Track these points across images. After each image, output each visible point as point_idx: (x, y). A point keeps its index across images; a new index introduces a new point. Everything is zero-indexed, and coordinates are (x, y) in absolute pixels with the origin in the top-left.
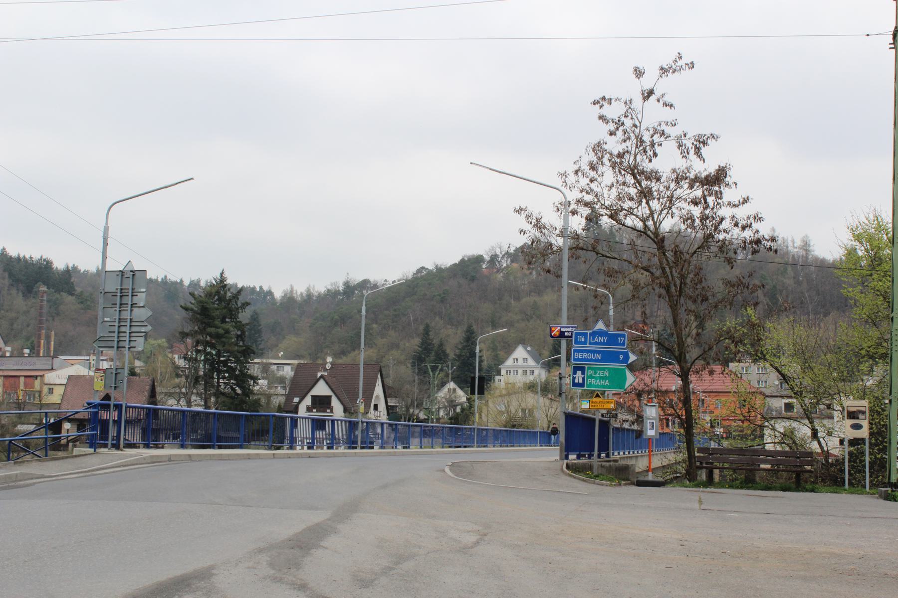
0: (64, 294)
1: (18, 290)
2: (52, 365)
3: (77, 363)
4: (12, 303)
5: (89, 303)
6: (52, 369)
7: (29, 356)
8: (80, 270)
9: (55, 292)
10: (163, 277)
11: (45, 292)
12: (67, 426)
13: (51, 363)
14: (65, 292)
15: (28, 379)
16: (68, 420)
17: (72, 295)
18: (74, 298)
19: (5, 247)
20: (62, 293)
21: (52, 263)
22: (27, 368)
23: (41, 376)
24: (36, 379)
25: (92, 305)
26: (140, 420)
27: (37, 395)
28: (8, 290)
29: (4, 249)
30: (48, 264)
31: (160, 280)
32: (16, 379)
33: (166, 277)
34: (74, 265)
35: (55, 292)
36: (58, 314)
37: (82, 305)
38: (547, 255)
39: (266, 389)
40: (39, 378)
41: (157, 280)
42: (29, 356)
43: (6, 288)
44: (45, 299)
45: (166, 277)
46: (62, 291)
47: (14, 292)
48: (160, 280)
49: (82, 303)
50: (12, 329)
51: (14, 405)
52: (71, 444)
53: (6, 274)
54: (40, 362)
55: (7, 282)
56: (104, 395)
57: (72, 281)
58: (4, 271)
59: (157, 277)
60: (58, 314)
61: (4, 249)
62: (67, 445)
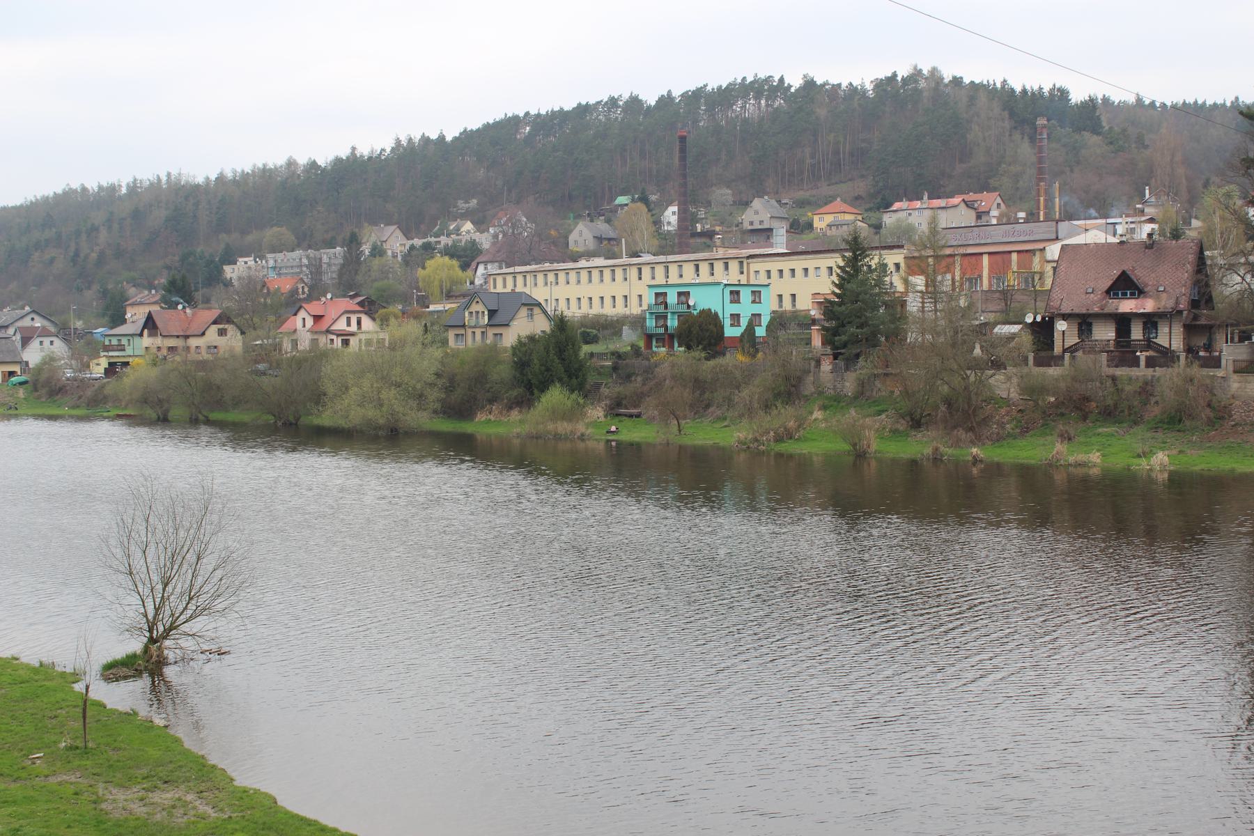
0: (1086, 134)
1: (1023, 134)
2: (1057, 232)
3: (1094, 228)
4: (1016, 152)
5: (1121, 143)
6: (1057, 239)
7: (1027, 221)
8: (1114, 102)
9: (1073, 132)
10: (1233, 99)
11: (1044, 127)
12: (1061, 326)
13: (1054, 229)
14: (1088, 131)
15: (1022, 255)
16: (1065, 317)
17: (1099, 134)
18: (1101, 138)
19: (1006, 79)
20: (1083, 132)
21: (1068, 92)
22: (1022, 239)
23: (1041, 250)
24: (1034, 255)
25: (1126, 145)
26: (1180, 312)
27: (1037, 278)
28: (1010, 135)
29: (1005, 81)
30: (1061, 94)
31: (1228, 104)
32: (1005, 256)
33: (1237, 98)
34: (1104, 96)
35: (1073, 132)
36: (1078, 163)
37: (1112, 146)
38: (966, 388)
39: (1158, 106)
40: (1038, 253)
41: (1224, 105)
42: (1027, 221)
43: (1007, 134)
44: (1045, 136)
45: (1237, 98)
46: (1084, 130)
47: (1017, 136)
48: (1228, 104)
49: (1111, 143)
50: (1018, 188)
51: (997, 295)
52: (1067, 355)
53: (1006, 114)
54: (1041, 229)
55: (1007, 124)
56: (1119, 273)
57: (1097, 114)
58: (1004, 110)
59: (1225, 101)
60: (1078, 163)
61: (1005, 81)
62: (1062, 357)
